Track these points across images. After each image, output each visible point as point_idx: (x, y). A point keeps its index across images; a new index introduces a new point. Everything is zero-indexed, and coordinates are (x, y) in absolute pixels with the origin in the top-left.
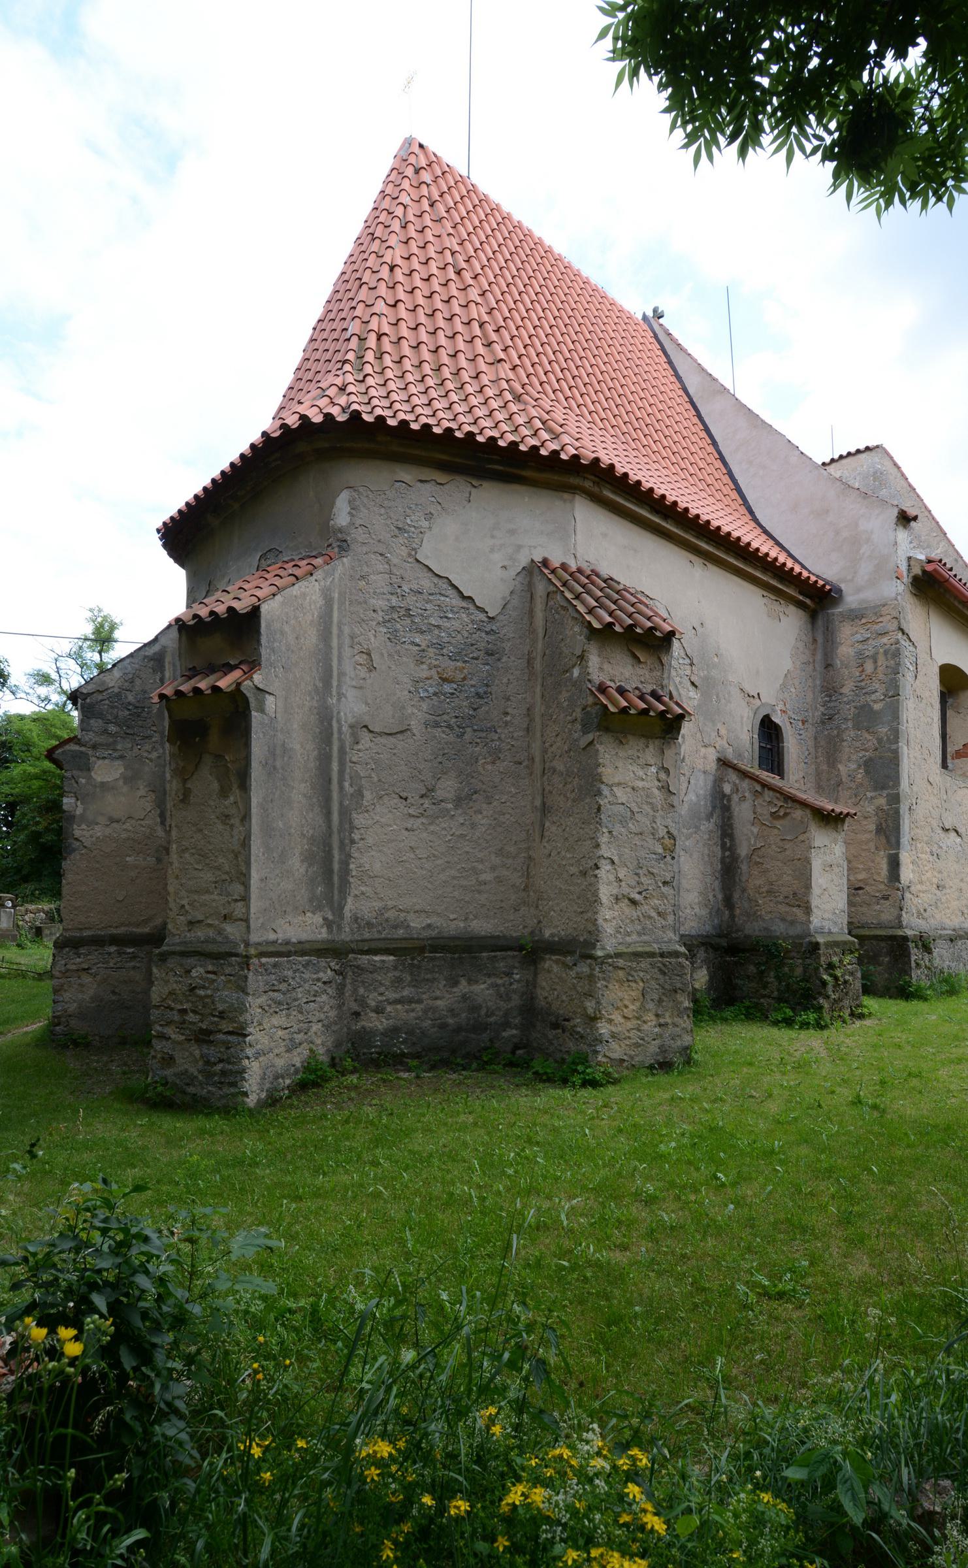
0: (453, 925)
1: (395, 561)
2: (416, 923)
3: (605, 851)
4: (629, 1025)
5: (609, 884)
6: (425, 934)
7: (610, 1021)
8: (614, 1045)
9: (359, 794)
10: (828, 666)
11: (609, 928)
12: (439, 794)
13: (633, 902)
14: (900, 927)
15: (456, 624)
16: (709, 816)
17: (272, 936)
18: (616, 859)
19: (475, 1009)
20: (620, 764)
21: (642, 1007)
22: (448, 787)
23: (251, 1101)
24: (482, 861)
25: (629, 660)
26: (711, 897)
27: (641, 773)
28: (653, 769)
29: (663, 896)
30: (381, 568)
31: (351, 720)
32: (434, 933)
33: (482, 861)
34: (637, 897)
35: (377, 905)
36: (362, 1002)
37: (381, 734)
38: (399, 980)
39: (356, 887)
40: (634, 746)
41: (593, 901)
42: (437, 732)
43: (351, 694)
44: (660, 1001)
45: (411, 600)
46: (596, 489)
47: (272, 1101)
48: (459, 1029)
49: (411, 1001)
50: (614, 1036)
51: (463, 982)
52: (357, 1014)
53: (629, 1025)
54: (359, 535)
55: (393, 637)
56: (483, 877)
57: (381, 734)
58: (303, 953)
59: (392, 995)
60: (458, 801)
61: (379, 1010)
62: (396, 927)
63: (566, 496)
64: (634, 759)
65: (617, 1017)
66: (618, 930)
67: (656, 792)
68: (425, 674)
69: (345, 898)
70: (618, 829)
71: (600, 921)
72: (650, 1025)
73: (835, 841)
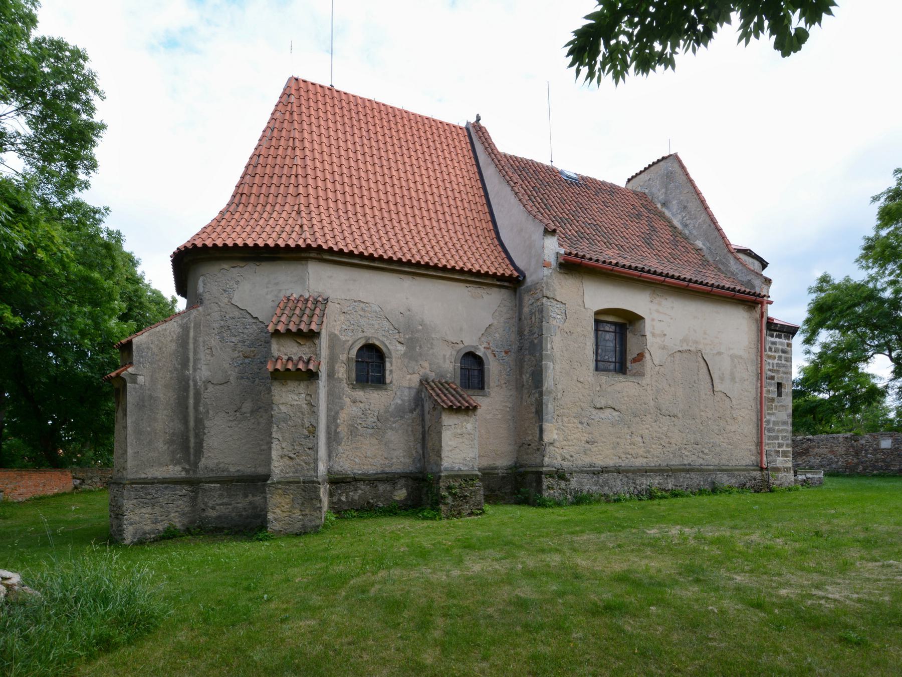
0: (249, 470)
1: (222, 305)
2: (232, 469)
3: (274, 435)
4: (285, 515)
5: (277, 450)
6: (236, 474)
7: (274, 513)
8: (275, 523)
9: (208, 412)
10: (520, 319)
11: (277, 471)
12: (243, 410)
13: (291, 458)
14: (543, 466)
15: (251, 331)
16: (411, 411)
17: (143, 476)
18: (281, 439)
19: (255, 508)
20: (284, 394)
21: (292, 507)
22: (247, 406)
23: (127, 542)
24: (262, 440)
25: (295, 344)
26: (414, 452)
27: (296, 398)
28: (303, 395)
29: (308, 455)
30: (216, 309)
31: (203, 379)
32: (240, 474)
33: (262, 440)
34: (293, 456)
35: (216, 461)
36: (206, 504)
37: (217, 384)
38: (222, 495)
39: (206, 454)
40: (292, 385)
41: (269, 460)
42: (242, 381)
43: (204, 368)
44: (303, 504)
45: (230, 322)
46: (319, 256)
47: (141, 542)
48: (247, 517)
49: (227, 504)
50: (275, 519)
51: (250, 496)
52: (204, 510)
53: (285, 515)
54: (206, 296)
55: (222, 339)
56: (263, 447)
57: (217, 384)
58: (163, 483)
59: (218, 501)
60: (252, 412)
61: (213, 508)
62: (223, 471)
63: (303, 262)
64: (293, 392)
65: (278, 511)
66: (282, 471)
67: (305, 406)
68: (237, 355)
69: (200, 459)
70: (282, 424)
71: (272, 467)
72: (297, 514)
73: (468, 422)
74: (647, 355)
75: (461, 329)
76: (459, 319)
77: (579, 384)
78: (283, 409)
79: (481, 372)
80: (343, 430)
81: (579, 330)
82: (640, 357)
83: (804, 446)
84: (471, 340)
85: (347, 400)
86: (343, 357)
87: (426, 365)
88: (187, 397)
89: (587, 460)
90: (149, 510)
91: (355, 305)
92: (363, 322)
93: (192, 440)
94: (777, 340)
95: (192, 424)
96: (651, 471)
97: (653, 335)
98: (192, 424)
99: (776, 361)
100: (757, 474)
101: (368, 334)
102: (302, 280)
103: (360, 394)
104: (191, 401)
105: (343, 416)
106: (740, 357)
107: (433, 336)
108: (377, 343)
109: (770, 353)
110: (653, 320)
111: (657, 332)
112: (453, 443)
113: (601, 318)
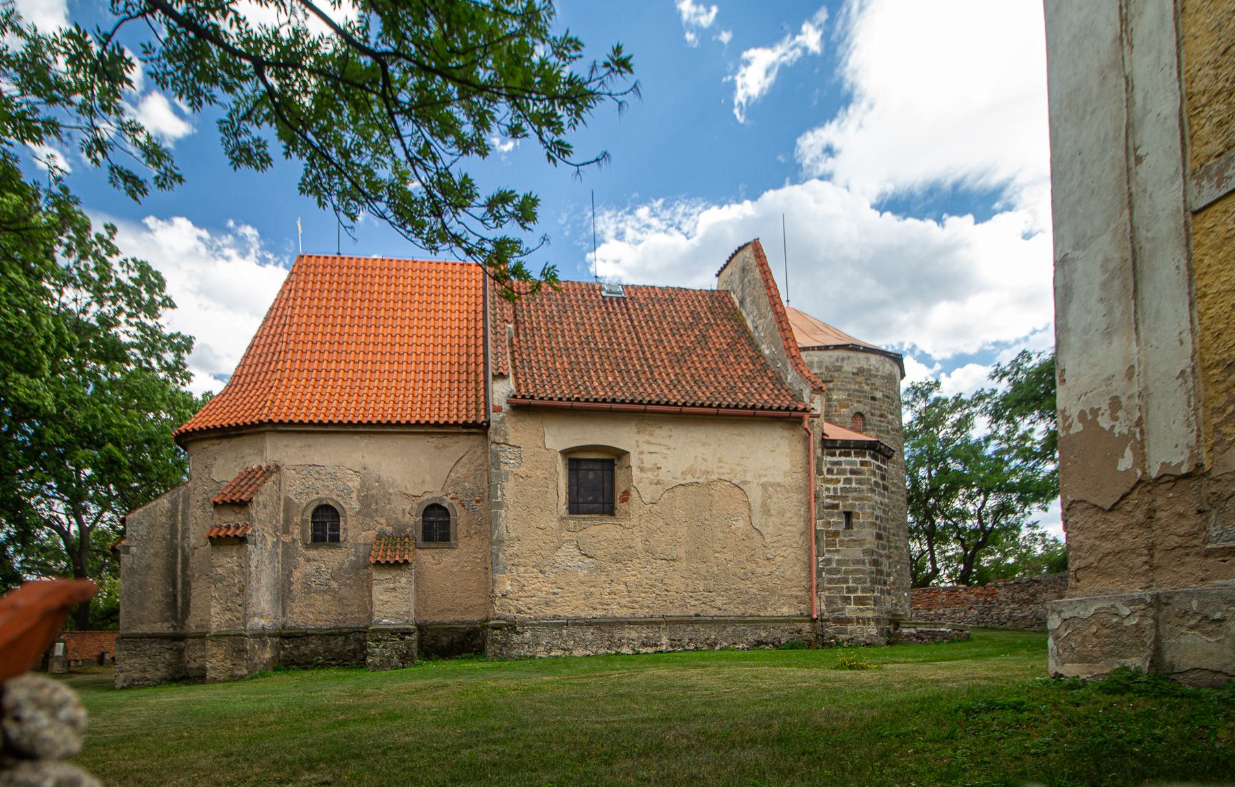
39: (193, 612)
64: (226, 556)
72: (229, 664)
74: (634, 493)
75: (423, 482)
76: (407, 474)
77: (539, 532)
78: (220, 570)
79: (446, 525)
80: (296, 587)
81: (538, 473)
82: (626, 495)
83: (1031, 590)
84: (433, 491)
85: (301, 559)
86: (297, 519)
87: (383, 521)
88: (176, 563)
89: (550, 612)
90: (138, 660)
91: (339, 469)
92: (318, 484)
93: (180, 600)
94: (843, 459)
95: (179, 586)
96: (636, 623)
97: (642, 469)
98: (179, 586)
99: (841, 485)
100: (807, 627)
101: (324, 494)
102: (261, 452)
103: (313, 553)
104: (179, 566)
105: (297, 574)
106: (779, 485)
107: (391, 491)
108: (331, 503)
109: (829, 477)
110: (642, 453)
111: (647, 465)
112: (385, 597)
113: (574, 460)
